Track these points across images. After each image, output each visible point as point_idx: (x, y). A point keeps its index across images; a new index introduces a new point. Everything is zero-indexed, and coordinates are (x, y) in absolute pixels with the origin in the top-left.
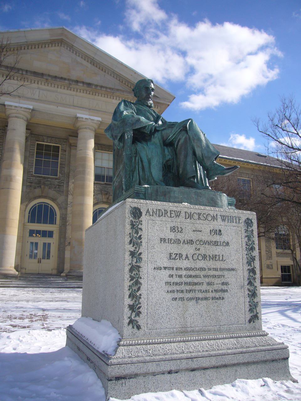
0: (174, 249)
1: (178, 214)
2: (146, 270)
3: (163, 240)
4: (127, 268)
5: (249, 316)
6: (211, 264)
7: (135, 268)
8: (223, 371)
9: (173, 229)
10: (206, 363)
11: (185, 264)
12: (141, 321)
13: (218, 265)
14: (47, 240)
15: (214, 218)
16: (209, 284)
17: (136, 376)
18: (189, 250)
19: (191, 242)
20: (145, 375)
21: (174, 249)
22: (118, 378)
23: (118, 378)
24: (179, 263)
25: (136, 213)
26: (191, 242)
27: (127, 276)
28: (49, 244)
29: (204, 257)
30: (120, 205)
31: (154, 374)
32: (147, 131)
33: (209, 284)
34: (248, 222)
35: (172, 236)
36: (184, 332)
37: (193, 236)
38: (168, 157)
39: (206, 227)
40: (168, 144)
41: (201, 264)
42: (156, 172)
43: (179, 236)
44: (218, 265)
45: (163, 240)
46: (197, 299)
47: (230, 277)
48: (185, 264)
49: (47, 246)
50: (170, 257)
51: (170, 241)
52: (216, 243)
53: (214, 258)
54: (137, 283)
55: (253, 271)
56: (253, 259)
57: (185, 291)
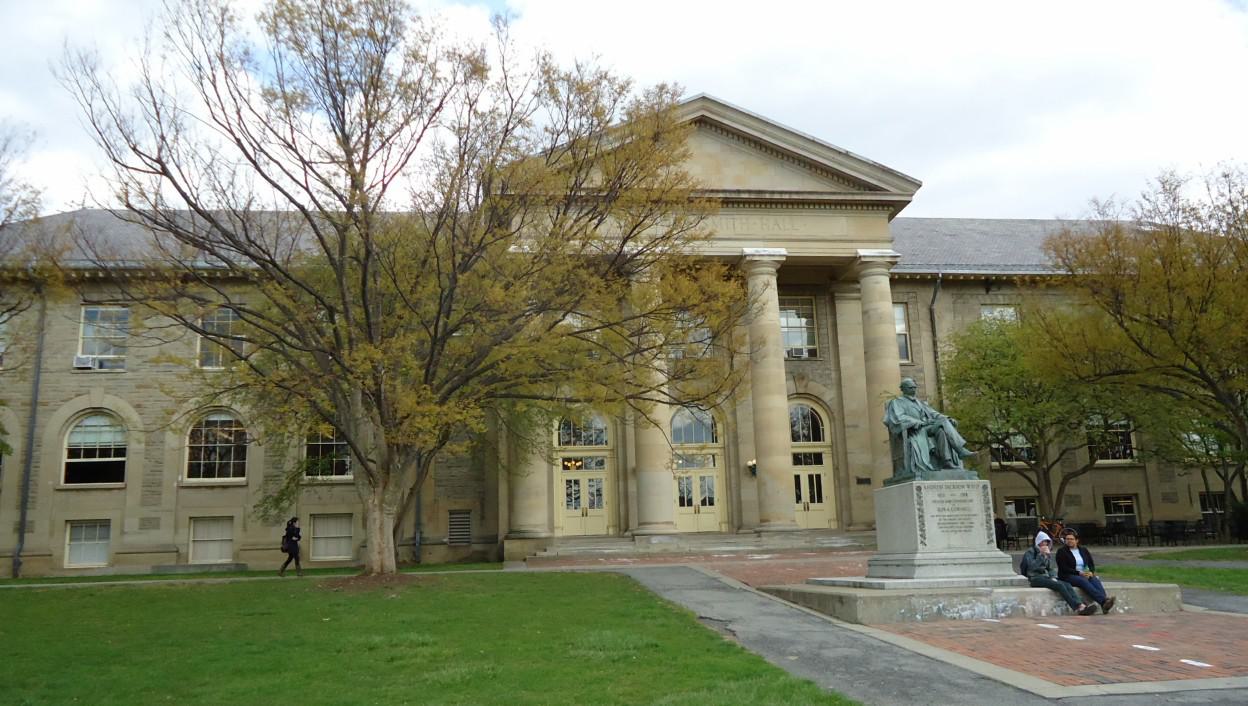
0: (940, 506)
1: (941, 487)
2: (927, 517)
3: (934, 501)
4: (917, 517)
5: (988, 540)
6: (962, 513)
7: (921, 517)
8: (971, 566)
9: (939, 495)
10: (961, 561)
11: (947, 513)
12: (926, 541)
13: (966, 513)
14: (814, 470)
15: (963, 487)
16: (962, 523)
17: (927, 565)
18: (947, 506)
19: (950, 501)
20: (932, 565)
21: (940, 506)
22: (919, 566)
23: (919, 566)
24: (944, 513)
25: (919, 489)
26: (950, 501)
27: (917, 520)
28: (818, 477)
29: (958, 509)
30: (966, 585)
31: (935, 565)
32: (917, 427)
33: (962, 523)
34: (985, 487)
35: (938, 499)
36: (949, 548)
37: (951, 498)
38: (933, 446)
39: (958, 493)
40: (930, 434)
41: (957, 513)
42: (926, 459)
43: (943, 499)
44: (966, 513)
45: (934, 501)
46: (956, 531)
47: (974, 519)
48: (947, 513)
49: (816, 482)
50: (939, 510)
51: (939, 502)
52: (965, 501)
53: (964, 509)
54: (923, 524)
55: (922, 530)
56: (989, 508)
57: (148, 512)
